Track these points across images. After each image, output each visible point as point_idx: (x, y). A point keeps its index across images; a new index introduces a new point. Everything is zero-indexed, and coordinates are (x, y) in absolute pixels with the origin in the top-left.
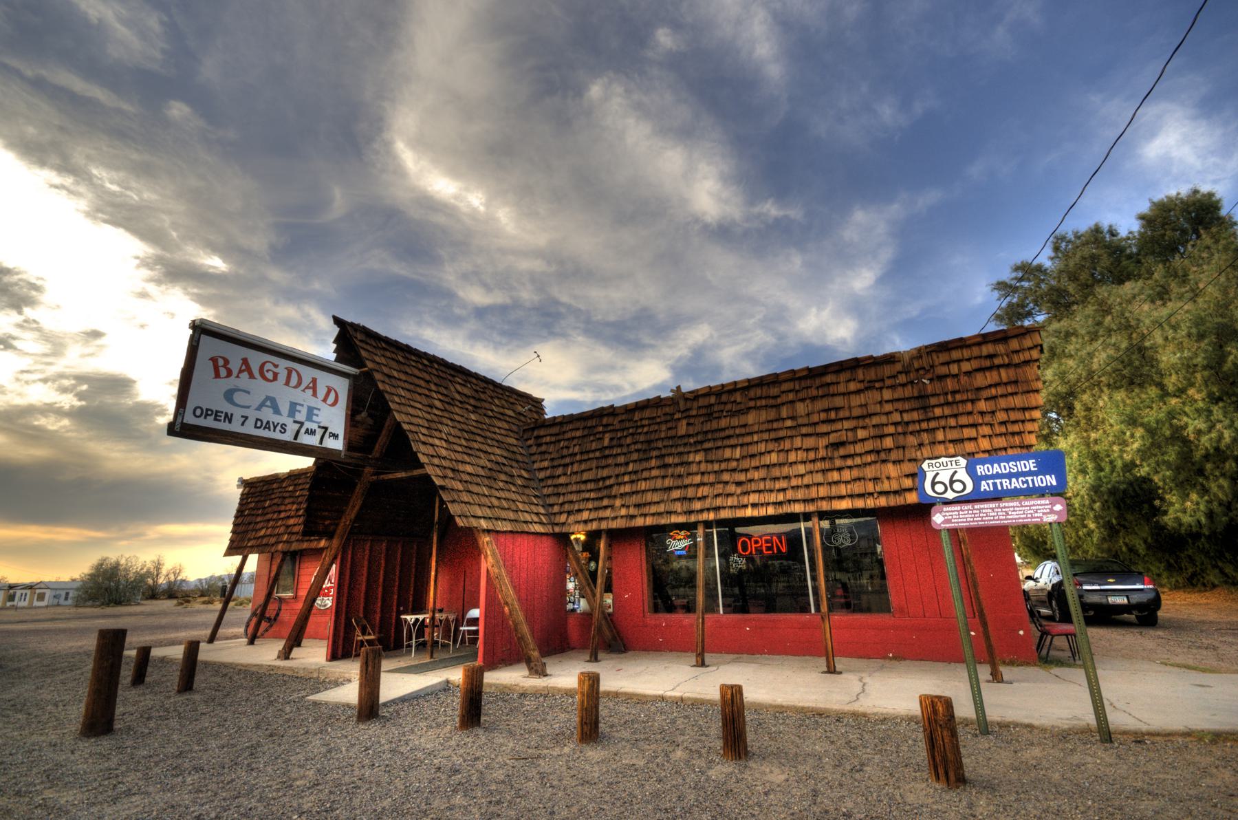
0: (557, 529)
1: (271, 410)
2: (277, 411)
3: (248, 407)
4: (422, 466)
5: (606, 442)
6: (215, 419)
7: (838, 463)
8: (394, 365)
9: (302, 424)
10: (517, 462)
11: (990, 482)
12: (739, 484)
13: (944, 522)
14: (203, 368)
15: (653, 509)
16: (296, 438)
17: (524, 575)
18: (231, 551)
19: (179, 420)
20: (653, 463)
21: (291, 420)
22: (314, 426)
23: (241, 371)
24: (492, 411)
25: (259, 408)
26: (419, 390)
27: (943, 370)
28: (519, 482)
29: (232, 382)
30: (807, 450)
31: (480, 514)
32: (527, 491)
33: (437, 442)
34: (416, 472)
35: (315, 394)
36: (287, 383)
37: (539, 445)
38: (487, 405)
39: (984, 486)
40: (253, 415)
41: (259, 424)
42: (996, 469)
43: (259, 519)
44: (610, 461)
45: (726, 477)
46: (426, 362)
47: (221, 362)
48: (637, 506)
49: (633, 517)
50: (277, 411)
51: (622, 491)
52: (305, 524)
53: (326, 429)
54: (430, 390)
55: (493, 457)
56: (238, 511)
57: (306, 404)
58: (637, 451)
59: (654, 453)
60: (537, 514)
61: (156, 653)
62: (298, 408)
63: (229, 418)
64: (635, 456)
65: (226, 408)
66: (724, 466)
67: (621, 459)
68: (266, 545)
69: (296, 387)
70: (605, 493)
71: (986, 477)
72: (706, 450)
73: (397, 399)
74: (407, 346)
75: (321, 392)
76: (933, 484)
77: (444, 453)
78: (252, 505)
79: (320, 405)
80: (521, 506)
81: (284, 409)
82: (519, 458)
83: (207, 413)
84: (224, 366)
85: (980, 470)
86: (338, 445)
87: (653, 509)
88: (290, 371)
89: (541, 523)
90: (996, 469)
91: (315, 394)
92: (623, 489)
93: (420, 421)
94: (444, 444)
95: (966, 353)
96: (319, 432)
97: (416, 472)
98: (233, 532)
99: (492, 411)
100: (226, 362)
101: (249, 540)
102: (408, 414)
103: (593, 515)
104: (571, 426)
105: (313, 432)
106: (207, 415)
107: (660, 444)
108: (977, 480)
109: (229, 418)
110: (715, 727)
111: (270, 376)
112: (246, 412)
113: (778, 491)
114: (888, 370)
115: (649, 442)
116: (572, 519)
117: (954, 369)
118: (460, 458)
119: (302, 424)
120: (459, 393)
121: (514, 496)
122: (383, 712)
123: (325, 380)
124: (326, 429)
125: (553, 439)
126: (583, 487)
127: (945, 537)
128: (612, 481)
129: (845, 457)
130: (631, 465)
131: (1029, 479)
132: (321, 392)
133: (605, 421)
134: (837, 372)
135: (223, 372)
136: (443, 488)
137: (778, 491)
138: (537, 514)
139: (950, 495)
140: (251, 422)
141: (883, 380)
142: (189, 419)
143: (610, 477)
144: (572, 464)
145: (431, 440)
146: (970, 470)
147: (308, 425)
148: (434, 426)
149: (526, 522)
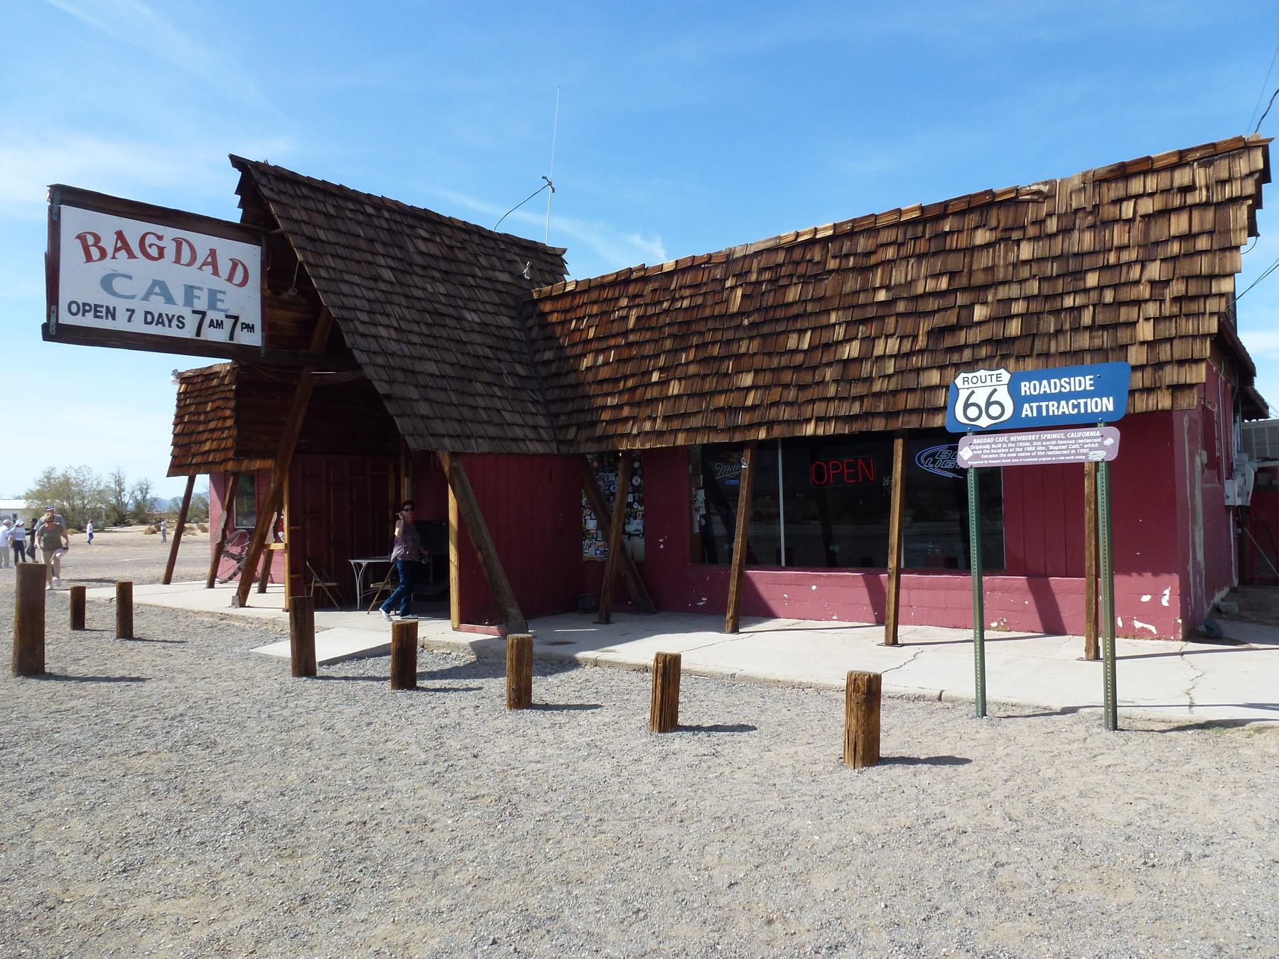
0: (564, 449)
1: (161, 299)
2: (169, 300)
3: (133, 297)
4: (359, 367)
6: (96, 316)
8: (319, 219)
9: (203, 314)
10: (510, 352)
11: (1034, 405)
12: (802, 387)
13: (970, 459)
14: (71, 252)
16: (198, 334)
18: (175, 470)
19: (53, 320)
21: (189, 310)
23: (117, 250)
24: (474, 276)
25: (146, 298)
26: (357, 255)
27: (1109, 212)
28: (510, 382)
29: (108, 265)
31: (443, 431)
32: (523, 395)
33: (383, 332)
35: (216, 272)
36: (178, 261)
38: (465, 269)
39: (1027, 411)
40: (141, 307)
41: (149, 319)
43: (201, 428)
45: (787, 377)
46: (370, 210)
47: (90, 240)
50: (169, 300)
51: (648, 396)
52: (238, 442)
53: (236, 318)
54: (374, 254)
55: (470, 348)
56: (177, 416)
57: (206, 287)
60: (535, 427)
61: (90, 594)
62: (196, 292)
63: (111, 313)
65: (106, 300)
66: (784, 361)
68: (213, 463)
69: (189, 265)
71: (1031, 399)
72: (763, 336)
73: (323, 273)
74: (341, 187)
75: (224, 267)
76: (967, 406)
77: (394, 347)
78: (192, 409)
79: (226, 286)
80: (508, 417)
81: (178, 295)
82: (514, 346)
83: (84, 308)
84: (96, 245)
85: (1026, 388)
86: (254, 339)
88: (179, 243)
89: (540, 440)
90: (1045, 387)
91: (216, 272)
93: (358, 303)
94: (394, 334)
95: (1152, 183)
96: (228, 323)
98: (175, 444)
99: (474, 276)
100: (97, 238)
101: (194, 456)
104: (585, 298)
105: (219, 325)
106: (85, 311)
107: (701, 327)
108: (1018, 400)
109: (111, 313)
110: (837, 719)
111: (154, 252)
112: (131, 304)
113: (854, 399)
115: (689, 323)
116: (584, 434)
117: (1128, 210)
119: (203, 314)
120: (421, 253)
121: (498, 404)
122: (321, 671)
123: (229, 249)
124: (236, 318)
127: (971, 478)
129: (950, 350)
130: (662, 358)
131: (1082, 401)
132: (224, 267)
133: (632, 289)
134: (961, 213)
135: (95, 253)
136: (388, 397)
137: (854, 399)
138: (535, 427)
139: (984, 422)
140: (139, 316)
141: (1023, 228)
142: (65, 318)
145: (373, 330)
146: (1013, 389)
147: (212, 315)
148: (377, 307)
149: (515, 440)
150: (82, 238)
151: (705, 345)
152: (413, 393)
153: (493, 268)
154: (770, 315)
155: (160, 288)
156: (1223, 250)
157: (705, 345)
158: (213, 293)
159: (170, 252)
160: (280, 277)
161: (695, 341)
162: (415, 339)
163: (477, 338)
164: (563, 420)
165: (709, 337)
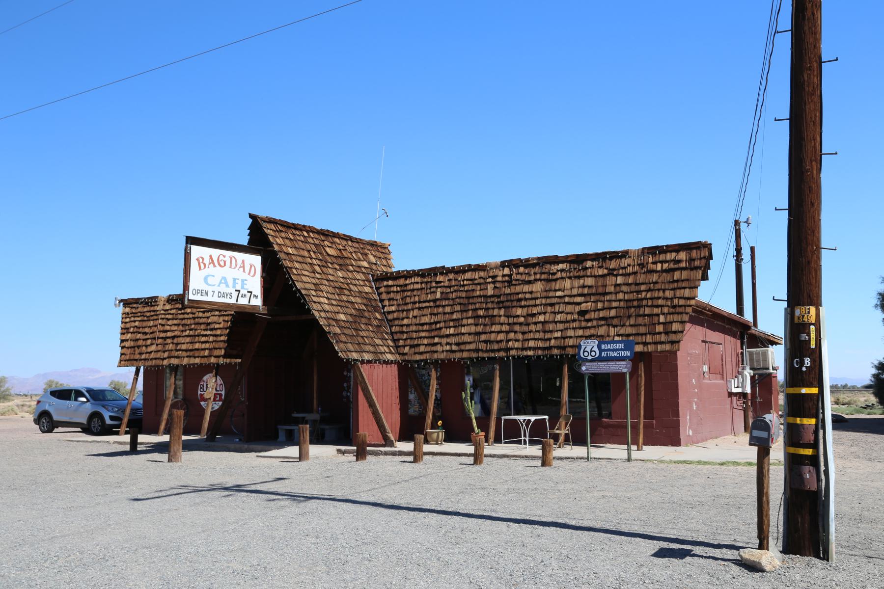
2: (227, 286)
5: (438, 296)
7: (584, 324)
9: (239, 291)
12: (523, 333)
15: (468, 347)
24: (352, 265)
30: (567, 313)
33: (322, 300)
34: (304, 317)
35: (244, 271)
39: (603, 354)
42: (609, 347)
44: (441, 309)
45: (517, 328)
47: (201, 260)
48: (457, 344)
49: (454, 352)
50: (227, 286)
58: (460, 304)
59: (470, 307)
64: (458, 308)
67: (448, 309)
70: (436, 333)
81: (230, 283)
85: (603, 347)
87: (468, 347)
89: (391, 353)
90: (609, 347)
91: (244, 271)
97: (304, 317)
99: (352, 265)
100: (203, 259)
102: (304, 280)
103: (428, 349)
108: (601, 351)
109: (207, 293)
114: (625, 262)
118: (336, 310)
119: (239, 291)
125: (399, 289)
126: (421, 328)
128: (442, 325)
139: (590, 358)
140: (216, 294)
143: (440, 322)
144: (413, 310)
146: (599, 346)
147: (243, 292)
153: (360, 260)
154: (509, 298)
155: (224, 281)
158: (243, 281)
159: (228, 263)
160: (275, 276)
164: (401, 343)
165: (478, 306)
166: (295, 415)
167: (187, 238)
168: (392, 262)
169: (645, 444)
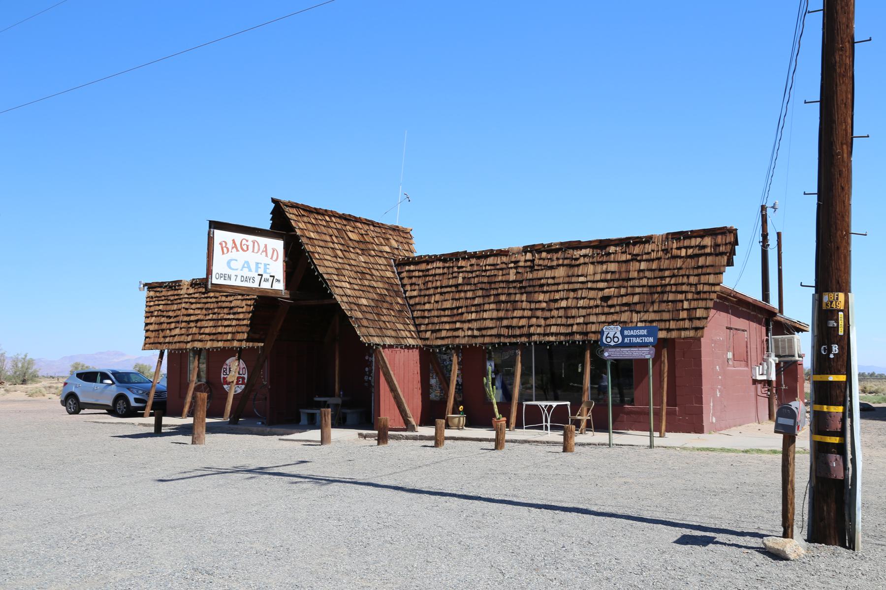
2: (250, 270)
5: (460, 281)
7: (606, 310)
12: (546, 319)
15: (490, 332)
17: (20, 365)
20: (492, 299)
22: (268, 277)
24: (374, 250)
27: (675, 252)
30: (590, 299)
34: (326, 302)
35: (267, 255)
37: (410, 278)
39: (626, 340)
42: (632, 333)
44: (462, 295)
45: (539, 313)
47: (224, 244)
48: (479, 329)
50: (250, 270)
58: (481, 289)
59: (492, 292)
64: (480, 293)
65: (228, 271)
67: (470, 295)
81: (253, 267)
85: (626, 333)
87: (490, 332)
89: (412, 338)
90: (632, 333)
91: (267, 255)
92: (469, 317)
97: (326, 302)
99: (374, 250)
100: (226, 243)
103: (450, 334)
108: (624, 337)
109: (230, 278)
111: (245, 248)
112: (236, 273)
114: (649, 247)
125: (421, 274)
126: (442, 313)
128: (464, 310)
135: (225, 250)
139: (612, 344)
140: (239, 278)
143: (461, 307)
144: (435, 295)
146: (622, 332)
150: (221, 244)
151: (498, 295)
152: (360, 315)
153: (382, 245)
154: (531, 283)
155: (247, 265)
156: (717, 274)
157: (498, 295)
158: (265, 265)
160: (297, 260)
161: (495, 292)
162: (356, 287)
163: (380, 285)
164: (423, 328)
165: (500, 291)
166: (317, 399)
167: (211, 222)
168: (414, 247)
169: (668, 431)
